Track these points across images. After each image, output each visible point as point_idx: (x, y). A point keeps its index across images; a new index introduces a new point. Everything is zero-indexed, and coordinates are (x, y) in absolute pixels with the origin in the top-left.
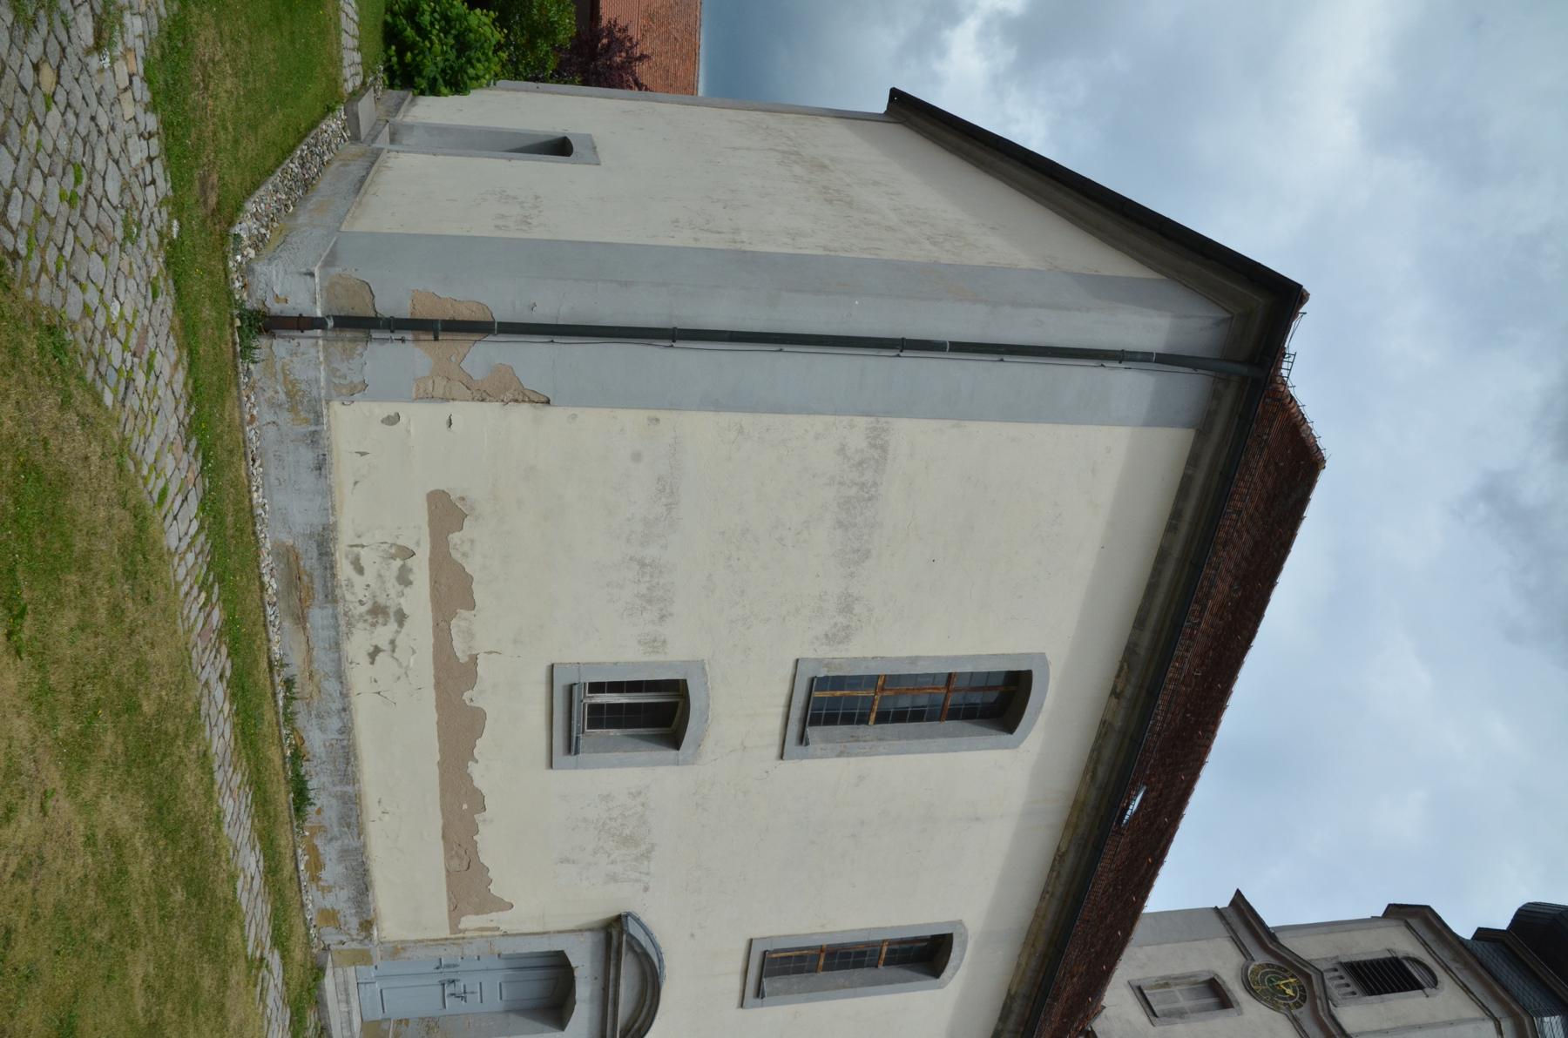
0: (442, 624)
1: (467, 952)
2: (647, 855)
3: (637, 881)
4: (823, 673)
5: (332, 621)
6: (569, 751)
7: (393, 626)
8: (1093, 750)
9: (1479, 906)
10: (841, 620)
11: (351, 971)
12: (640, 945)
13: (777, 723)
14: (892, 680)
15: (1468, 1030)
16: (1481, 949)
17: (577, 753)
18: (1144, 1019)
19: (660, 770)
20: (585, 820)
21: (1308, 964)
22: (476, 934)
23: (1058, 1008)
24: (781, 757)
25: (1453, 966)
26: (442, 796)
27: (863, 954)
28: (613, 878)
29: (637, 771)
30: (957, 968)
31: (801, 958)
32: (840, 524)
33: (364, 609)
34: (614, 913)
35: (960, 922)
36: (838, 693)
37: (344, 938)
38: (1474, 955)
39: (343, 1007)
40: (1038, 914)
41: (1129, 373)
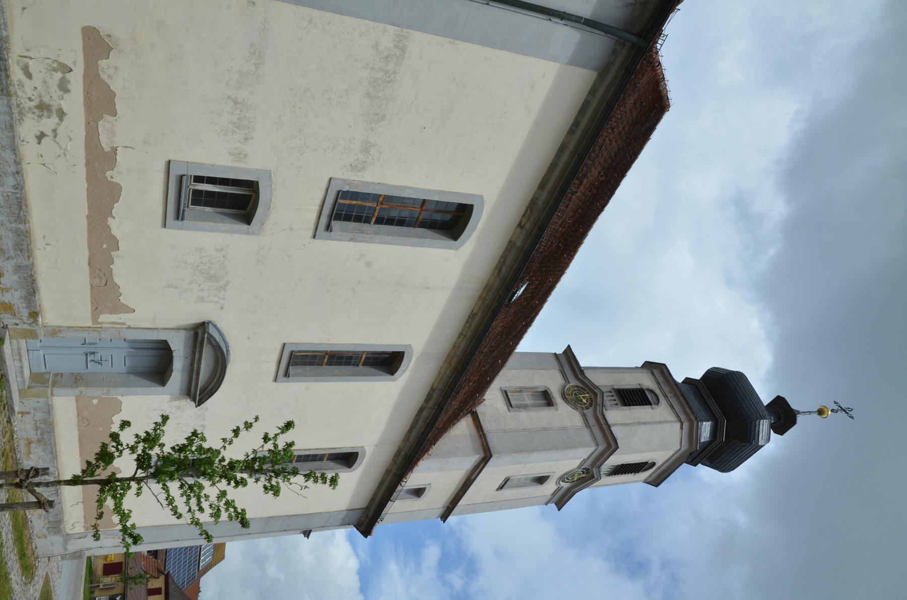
0: (92, 123)
1: (103, 336)
2: (223, 288)
3: (216, 302)
4: (346, 189)
5: (7, 109)
6: (177, 218)
7: (55, 119)
8: (502, 257)
9: (688, 368)
10: (362, 157)
11: (23, 342)
12: (215, 340)
13: (313, 216)
14: (389, 199)
15: (667, 426)
16: (685, 389)
17: (183, 219)
18: (505, 408)
19: (237, 237)
20: (185, 262)
21: (597, 387)
22: (110, 326)
23: (460, 398)
24: (314, 237)
25: (669, 395)
26: (89, 237)
27: (351, 358)
28: (202, 299)
29: (222, 235)
30: (404, 371)
31: (314, 357)
32: (369, 95)
33: (32, 104)
34: (201, 321)
35: (410, 346)
36: (354, 202)
37: (18, 322)
38: (680, 391)
39: (18, 364)
40: (455, 346)
41: (565, 28)
